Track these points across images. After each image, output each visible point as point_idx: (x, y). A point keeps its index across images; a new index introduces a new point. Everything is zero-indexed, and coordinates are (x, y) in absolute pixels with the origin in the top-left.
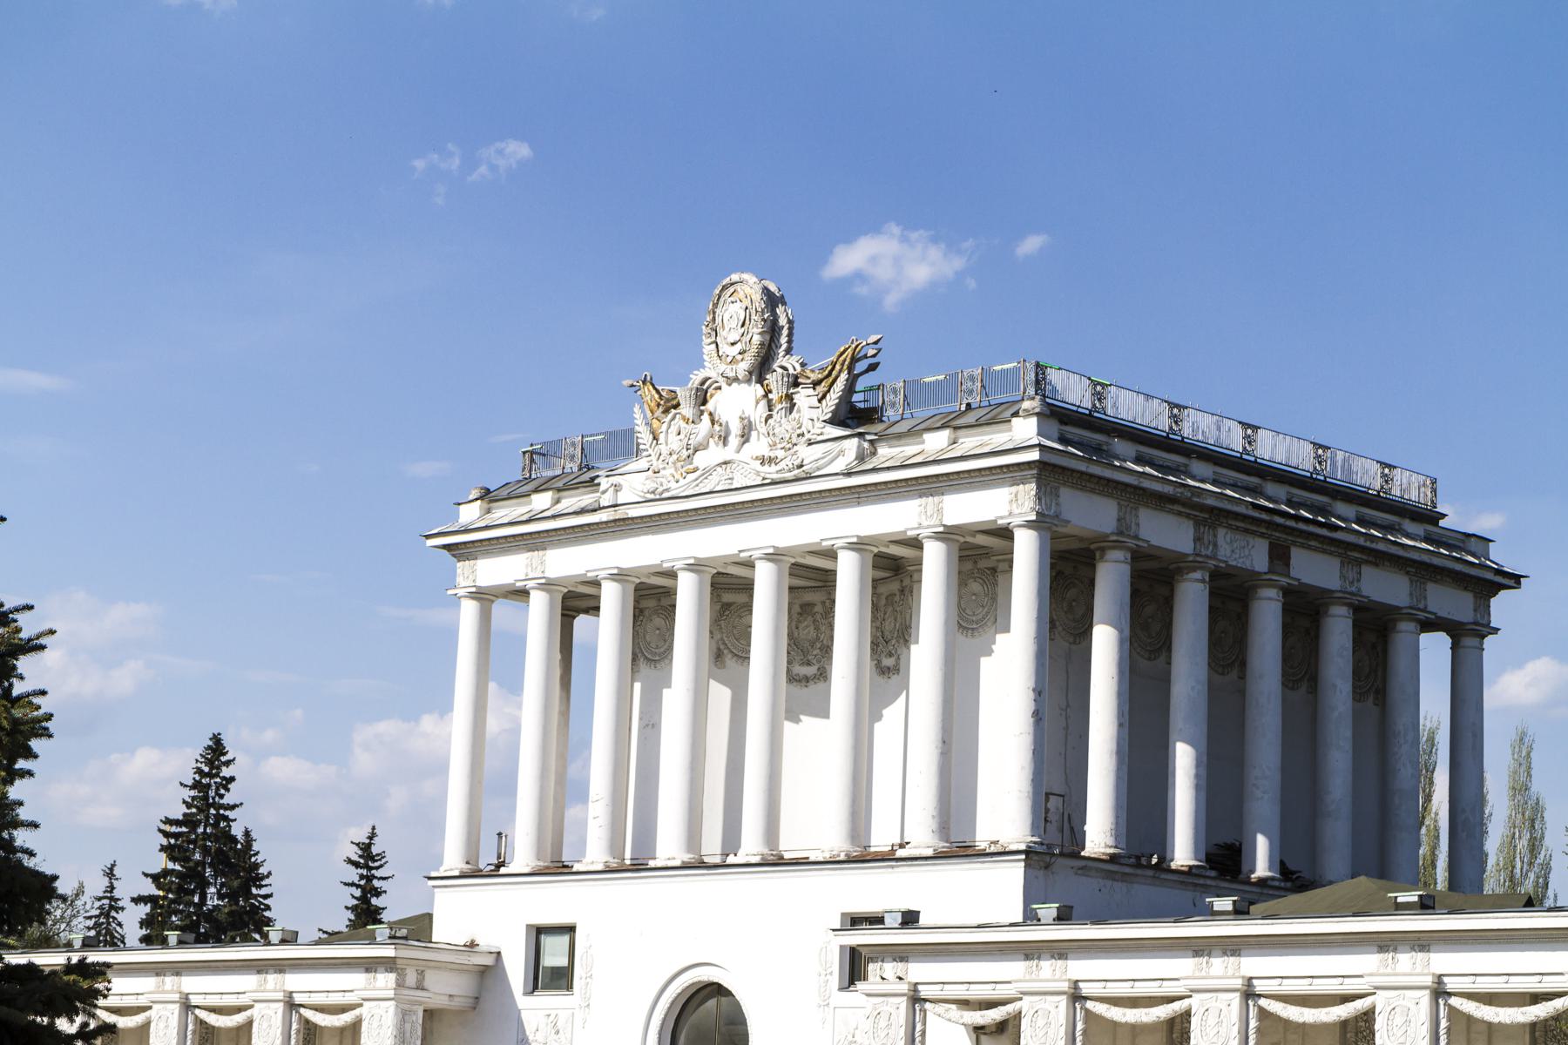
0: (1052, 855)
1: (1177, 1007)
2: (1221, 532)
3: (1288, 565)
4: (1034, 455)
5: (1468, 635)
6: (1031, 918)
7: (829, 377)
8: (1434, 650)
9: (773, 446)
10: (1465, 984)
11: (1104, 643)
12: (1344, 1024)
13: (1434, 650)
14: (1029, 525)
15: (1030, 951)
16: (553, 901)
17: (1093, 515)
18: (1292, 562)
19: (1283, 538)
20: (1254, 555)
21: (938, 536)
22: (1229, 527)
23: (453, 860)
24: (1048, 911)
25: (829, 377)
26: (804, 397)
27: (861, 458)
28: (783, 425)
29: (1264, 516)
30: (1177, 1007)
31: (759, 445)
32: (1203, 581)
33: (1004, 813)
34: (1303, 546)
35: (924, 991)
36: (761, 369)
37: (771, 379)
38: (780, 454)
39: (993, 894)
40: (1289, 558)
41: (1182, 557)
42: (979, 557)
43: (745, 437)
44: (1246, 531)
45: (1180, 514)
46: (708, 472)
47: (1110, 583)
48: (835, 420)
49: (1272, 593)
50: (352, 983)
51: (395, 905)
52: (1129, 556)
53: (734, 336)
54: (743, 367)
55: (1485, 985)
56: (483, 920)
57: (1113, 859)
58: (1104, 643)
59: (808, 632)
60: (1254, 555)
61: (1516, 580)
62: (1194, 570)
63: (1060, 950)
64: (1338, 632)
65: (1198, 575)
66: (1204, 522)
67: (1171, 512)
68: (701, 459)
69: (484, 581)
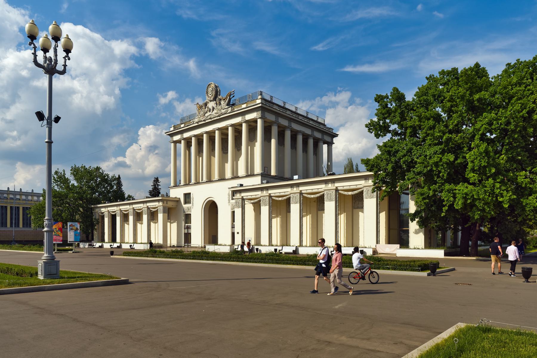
0: (265, 175)
4: (260, 105)
5: (330, 144)
6: (262, 183)
7: (226, 98)
8: (325, 147)
10: (341, 188)
11: (273, 142)
12: (317, 198)
13: (325, 147)
15: (262, 189)
16: (187, 190)
17: (271, 117)
21: (244, 122)
23: (172, 184)
24: (264, 181)
25: (226, 98)
26: (222, 102)
27: (232, 110)
28: (219, 107)
31: (215, 111)
33: (258, 169)
35: (244, 198)
36: (215, 99)
37: (217, 99)
39: (256, 181)
41: (286, 126)
42: (252, 126)
43: (213, 110)
46: (208, 116)
47: (275, 130)
48: (227, 105)
50: (156, 204)
51: (162, 192)
54: (212, 99)
56: (177, 193)
57: (275, 176)
58: (273, 142)
59: (224, 137)
63: (267, 188)
64: (311, 142)
68: (206, 115)
69: (174, 140)
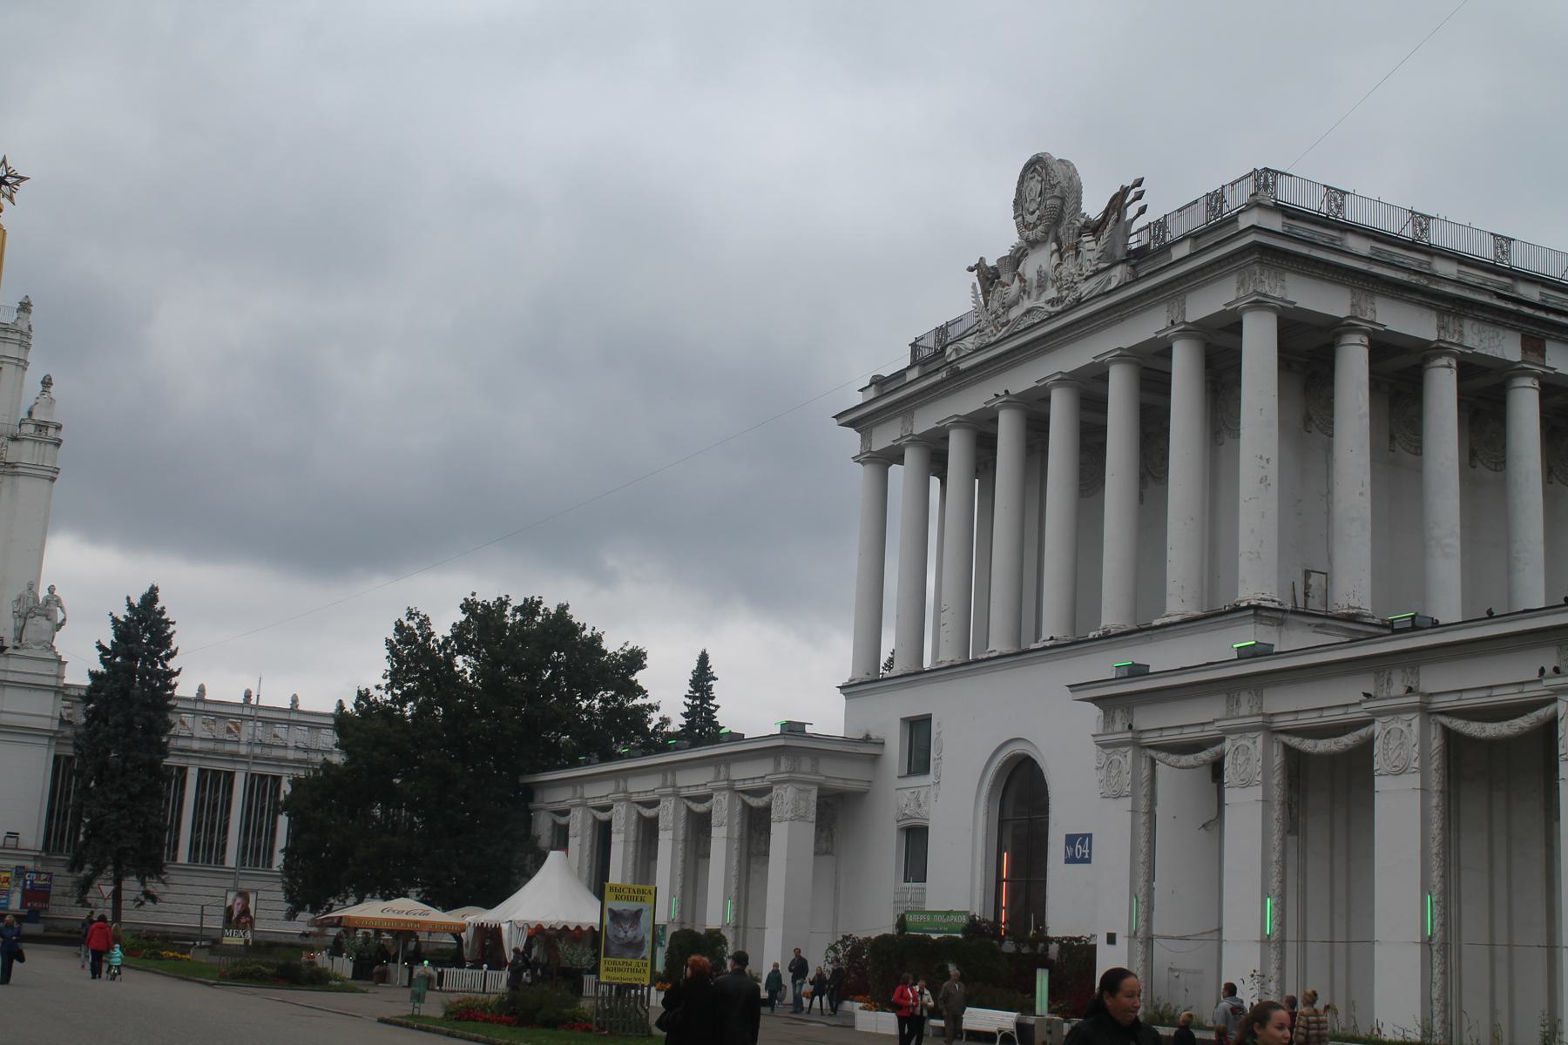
1: (1543, 713)
2: (1467, 324)
3: (1543, 356)
9: (1059, 290)
14: (143, 883)
18: (1547, 354)
19: (1538, 330)
20: (1508, 347)
22: (1476, 319)
29: (1510, 306)
30: (1543, 713)
32: (1449, 367)
34: (1557, 340)
38: (1064, 293)
40: (1544, 350)
43: (1041, 287)
44: (1494, 323)
45: (1420, 304)
49: (1528, 382)
52: (1366, 341)
53: (1033, 207)
55: (1471, 700)
60: (1508, 347)
61: (154, 590)
62: (1440, 356)
65: (1444, 361)
66: (1447, 312)
67: (1409, 301)
